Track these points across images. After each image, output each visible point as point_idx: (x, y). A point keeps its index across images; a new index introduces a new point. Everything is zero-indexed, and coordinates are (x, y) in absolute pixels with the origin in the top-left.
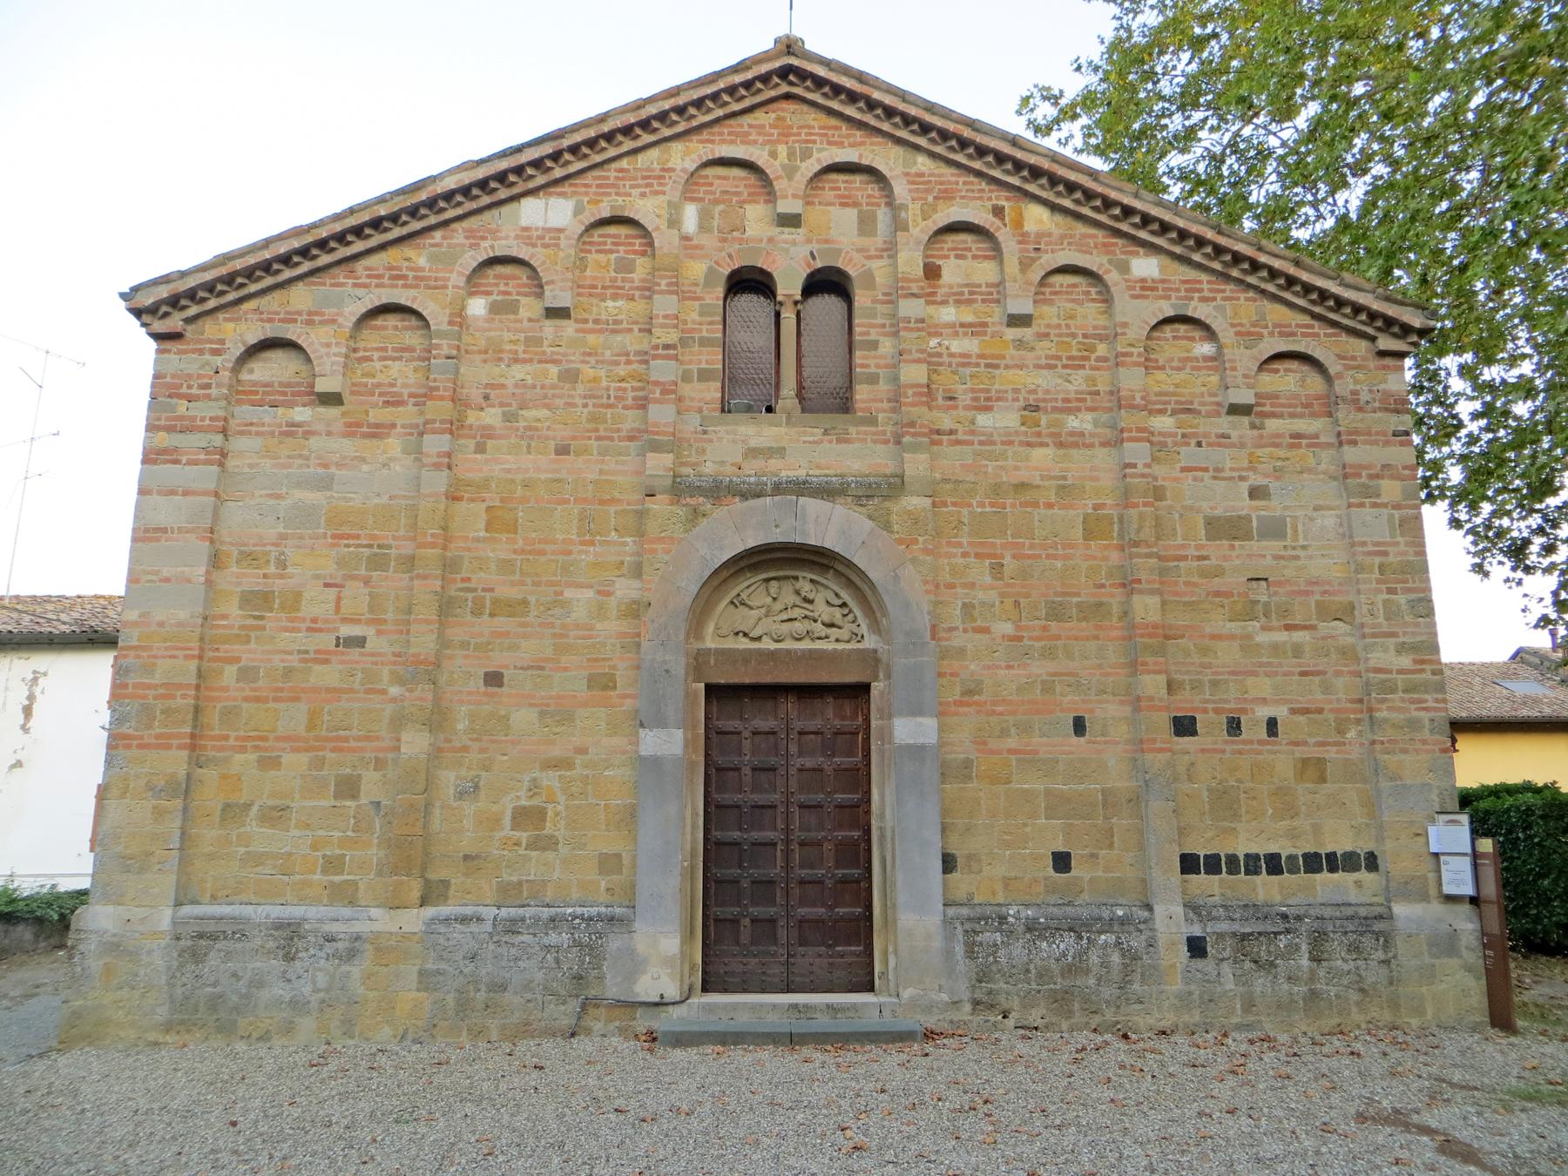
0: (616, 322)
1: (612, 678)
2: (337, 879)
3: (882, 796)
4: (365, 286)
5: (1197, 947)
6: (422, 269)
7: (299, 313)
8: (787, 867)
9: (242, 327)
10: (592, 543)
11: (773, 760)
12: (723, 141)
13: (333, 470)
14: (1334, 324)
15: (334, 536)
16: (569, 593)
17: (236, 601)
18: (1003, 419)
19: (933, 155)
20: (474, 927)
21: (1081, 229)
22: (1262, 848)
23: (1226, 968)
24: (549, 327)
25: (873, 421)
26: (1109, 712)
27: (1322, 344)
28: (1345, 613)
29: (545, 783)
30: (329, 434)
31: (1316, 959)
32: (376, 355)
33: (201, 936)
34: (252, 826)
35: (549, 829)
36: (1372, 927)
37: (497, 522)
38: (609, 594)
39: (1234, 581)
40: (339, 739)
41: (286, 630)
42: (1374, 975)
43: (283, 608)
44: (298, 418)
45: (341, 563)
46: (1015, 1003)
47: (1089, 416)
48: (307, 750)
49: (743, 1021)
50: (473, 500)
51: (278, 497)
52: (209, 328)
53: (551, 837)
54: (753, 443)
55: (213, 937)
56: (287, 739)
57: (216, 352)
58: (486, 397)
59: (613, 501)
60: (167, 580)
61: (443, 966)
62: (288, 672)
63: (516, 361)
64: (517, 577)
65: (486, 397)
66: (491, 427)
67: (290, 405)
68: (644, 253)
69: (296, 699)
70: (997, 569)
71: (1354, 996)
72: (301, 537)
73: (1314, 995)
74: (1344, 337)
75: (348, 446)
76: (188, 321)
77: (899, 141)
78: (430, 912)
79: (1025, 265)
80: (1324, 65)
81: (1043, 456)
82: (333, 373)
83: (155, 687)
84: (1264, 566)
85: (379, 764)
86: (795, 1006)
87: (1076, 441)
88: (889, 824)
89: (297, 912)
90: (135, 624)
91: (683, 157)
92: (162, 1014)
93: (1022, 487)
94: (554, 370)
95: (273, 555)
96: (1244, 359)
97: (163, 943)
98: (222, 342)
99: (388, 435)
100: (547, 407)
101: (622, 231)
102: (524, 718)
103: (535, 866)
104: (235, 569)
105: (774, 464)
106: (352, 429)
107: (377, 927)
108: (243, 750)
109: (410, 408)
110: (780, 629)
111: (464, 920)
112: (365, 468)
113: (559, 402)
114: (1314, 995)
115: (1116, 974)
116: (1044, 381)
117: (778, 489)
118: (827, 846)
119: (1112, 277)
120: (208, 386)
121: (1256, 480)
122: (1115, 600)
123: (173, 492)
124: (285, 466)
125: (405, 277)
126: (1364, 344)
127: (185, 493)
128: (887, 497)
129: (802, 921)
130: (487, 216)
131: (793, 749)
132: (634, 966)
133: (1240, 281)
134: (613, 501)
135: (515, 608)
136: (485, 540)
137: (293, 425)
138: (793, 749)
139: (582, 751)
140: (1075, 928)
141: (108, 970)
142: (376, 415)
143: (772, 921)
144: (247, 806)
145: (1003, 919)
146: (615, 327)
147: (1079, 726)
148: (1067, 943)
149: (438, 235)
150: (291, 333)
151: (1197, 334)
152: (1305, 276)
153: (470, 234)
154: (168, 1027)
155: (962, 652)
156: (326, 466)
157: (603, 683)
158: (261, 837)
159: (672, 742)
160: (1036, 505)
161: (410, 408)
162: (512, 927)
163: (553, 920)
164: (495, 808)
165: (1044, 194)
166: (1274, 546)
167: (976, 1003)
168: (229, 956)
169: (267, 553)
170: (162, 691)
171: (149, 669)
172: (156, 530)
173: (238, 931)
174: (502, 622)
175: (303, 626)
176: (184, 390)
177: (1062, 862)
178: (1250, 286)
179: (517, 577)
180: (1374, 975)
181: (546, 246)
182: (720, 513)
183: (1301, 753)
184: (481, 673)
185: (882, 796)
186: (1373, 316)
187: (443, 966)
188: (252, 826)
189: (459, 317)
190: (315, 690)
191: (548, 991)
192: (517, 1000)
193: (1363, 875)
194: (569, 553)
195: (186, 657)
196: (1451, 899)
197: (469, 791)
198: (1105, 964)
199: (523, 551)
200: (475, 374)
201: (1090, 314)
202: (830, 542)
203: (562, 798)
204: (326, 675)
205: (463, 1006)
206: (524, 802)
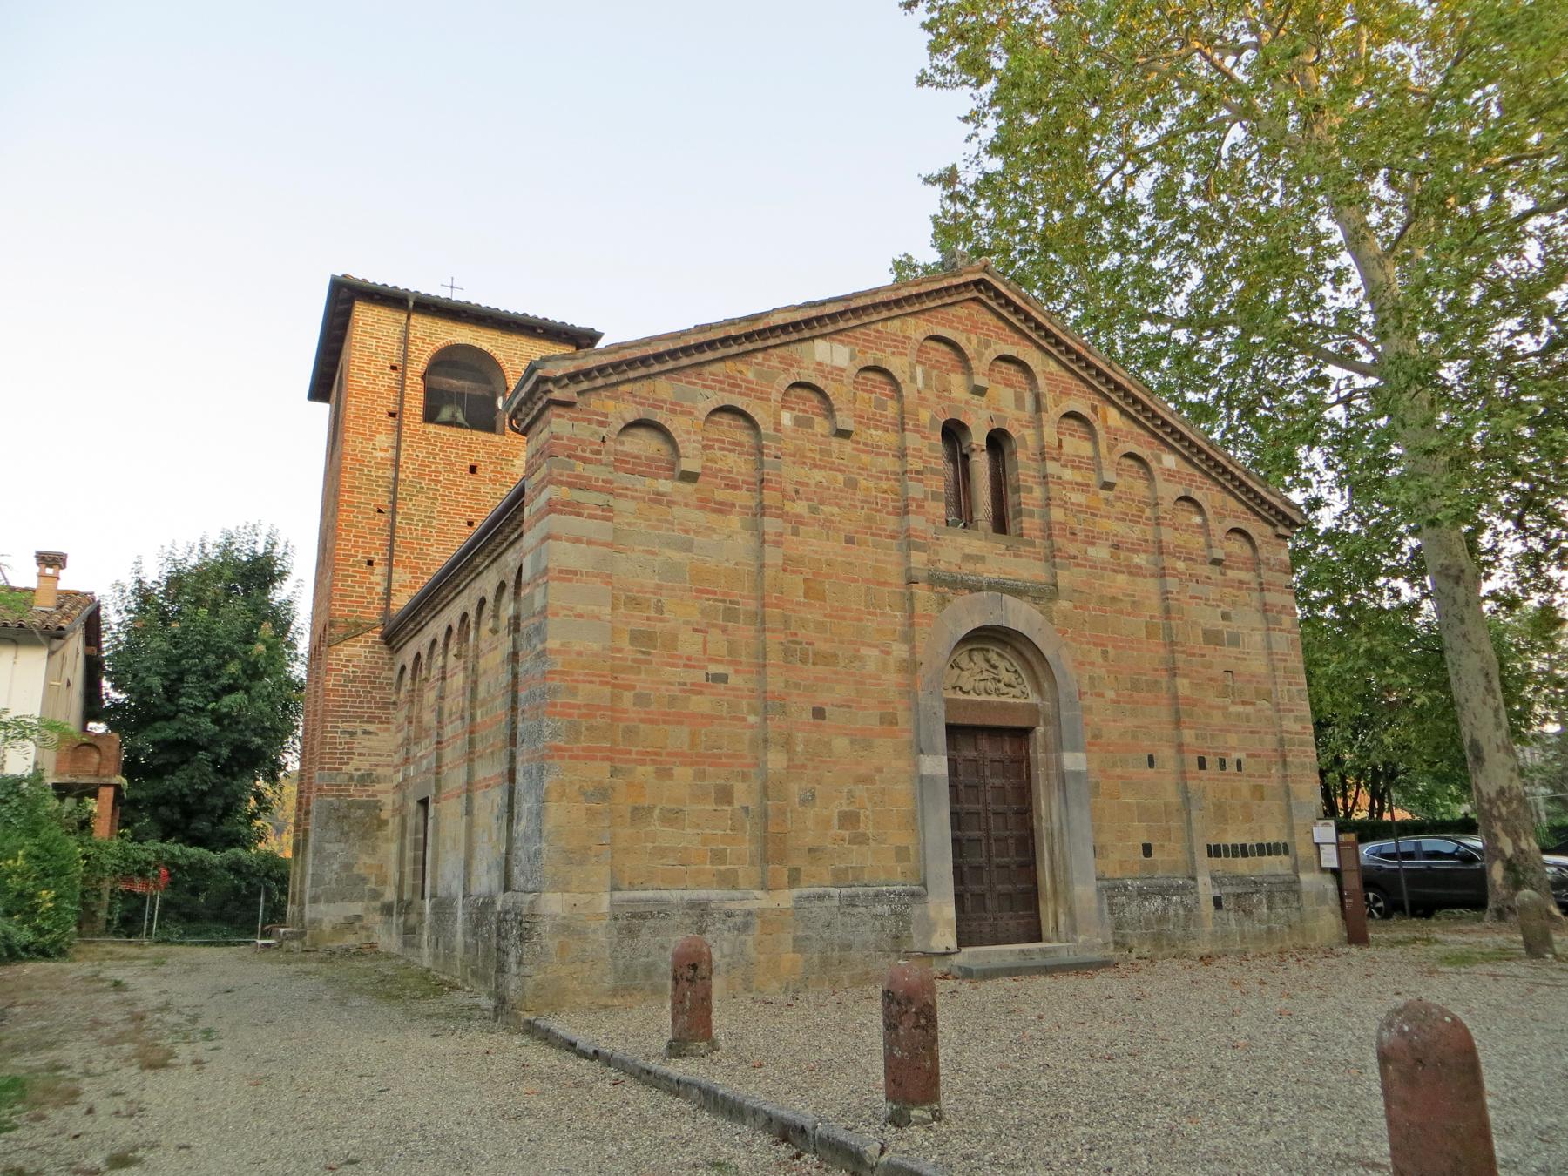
0: (879, 447)
1: (894, 716)
2: (722, 868)
3: (1049, 805)
4: (712, 388)
5: (1218, 903)
6: (750, 382)
7: (664, 401)
8: (989, 856)
9: (621, 406)
10: (874, 614)
11: (976, 780)
12: (938, 323)
13: (692, 535)
14: (1257, 514)
15: (697, 591)
16: (863, 651)
17: (627, 637)
18: (1100, 552)
19: (1059, 361)
20: (827, 903)
21: (1137, 430)
22: (1239, 841)
23: (1231, 914)
24: (835, 443)
25: (1032, 544)
26: (1166, 754)
27: (1256, 528)
28: (1267, 696)
29: (858, 794)
30: (686, 505)
31: (1270, 908)
32: (717, 445)
33: (633, 916)
34: (656, 827)
35: (862, 828)
36: (1291, 887)
37: (813, 592)
38: (888, 653)
39: (1217, 672)
40: (714, 756)
41: (668, 665)
42: (1295, 917)
43: (664, 646)
44: (662, 489)
45: (703, 612)
46: (1135, 942)
47: (1144, 556)
48: (692, 764)
49: (996, 962)
50: (794, 572)
51: (653, 553)
52: (595, 402)
53: (864, 834)
54: (967, 550)
55: (643, 917)
56: (676, 754)
57: (602, 424)
58: (797, 492)
59: (885, 583)
60: (580, 616)
61: (809, 933)
62: (673, 699)
63: (815, 466)
64: (828, 635)
65: (797, 492)
66: (800, 516)
67: (656, 477)
68: (892, 397)
69: (680, 723)
70: (1105, 654)
71: (1287, 930)
72: (673, 589)
73: (1270, 930)
74: (1261, 523)
75: (699, 517)
76: (579, 394)
77: (1040, 347)
78: (795, 892)
79: (1111, 448)
80: (1175, 327)
81: (1122, 579)
82: (694, 457)
83: (579, 707)
84: (1231, 663)
85: (745, 777)
86: (1022, 951)
87: (1134, 572)
88: (1056, 825)
89: (703, 894)
90: (558, 652)
91: (916, 329)
92: (609, 981)
93: (1114, 599)
94: (841, 477)
95: (653, 601)
96: (1219, 529)
97: (604, 923)
98: (606, 415)
99: (730, 513)
100: (838, 505)
101: (878, 377)
102: (840, 744)
103: (856, 856)
104: (622, 610)
105: (979, 567)
106: (703, 504)
107: (763, 904)
108: (642, 762)
109: (744, 492)
110: (997, 689)
111: (820, 897)
112: (715, 537)
113: (846, 503)
114: (1270, 930)
115: (1182, 923)
116: (1121, 528)
117: (990, 587)
118: (1010, 841)
119: (1154, 465)
120: (598, 452)
121: (1225, 608)
122: (1164, 679)
123: (578, 540)
124: (655, 528)
125: (739, 386)
126: (1270, 529)
127: (589, 543)
128: (1050, 600)
129: (1000, 895)
130: (792, 347)
131: (988, 773)
132: (929, 928)
133: (1215, 479)
134: (885, 583)
135: (828, 659)
136: (805, 605)
137: (658, 494)
138: (988, 773)
139: (880, 770)
140: (1162, 892)
141: (563, 948)
142: (721, 495)
143: (983, 895)
144: (651, 809)
145: (1126, 887)
146: (877, 451)
147: (1151, 761)
148: (1157, 903)
149: (760, 356)
150: (660, 417)
151: (1193, 509)
152: (1250, 483)
153: (782, 360)
154: (615, 993)
155: (1090, 709)
156: (686, 532)
157: (889, 720)
158: (666, 835)
159: (936, 765)
160: (1121, 612)
161: (744, 492)
162: (852, 901)
163: (877, 895)
164: (826, 812)
165: (1120, 403)
166: (1234, 650)
167: (1116, 943)
168: (656, 931)
169: (649, 600)
170: (584, 711)
171: (573, 692)
172: (568, 572)
173: (661, 911)
174: (821, 670)
175: (681, 662)
176: (579, 453)
177: (1147, 850)
178: (1219, 483)
179: (828, 635)
180: (1295, 917)
181: (834, 380)
182: (957, 600)
183: (1253, 781)
184: (810, 708)
185: (1049, 805)
186: (1279, 512)
187: (809, 933)
188: (656, 827)
189: (778, 426)
190: (693, 715)
191: (879, 948)
192: (859, 956)
193: (1283, 857)
194: (860, 620)
195: (602, 683)
196: (1323, 870)
197: (809, 799)
198: (1176, 915)
199: (830, 616)
200: (791, 472)
201: (1140, 487)
202: (1021, 627)
203: (869, 805)
204: (701, 704)
205: (825, 962)
206: (845, 808)
